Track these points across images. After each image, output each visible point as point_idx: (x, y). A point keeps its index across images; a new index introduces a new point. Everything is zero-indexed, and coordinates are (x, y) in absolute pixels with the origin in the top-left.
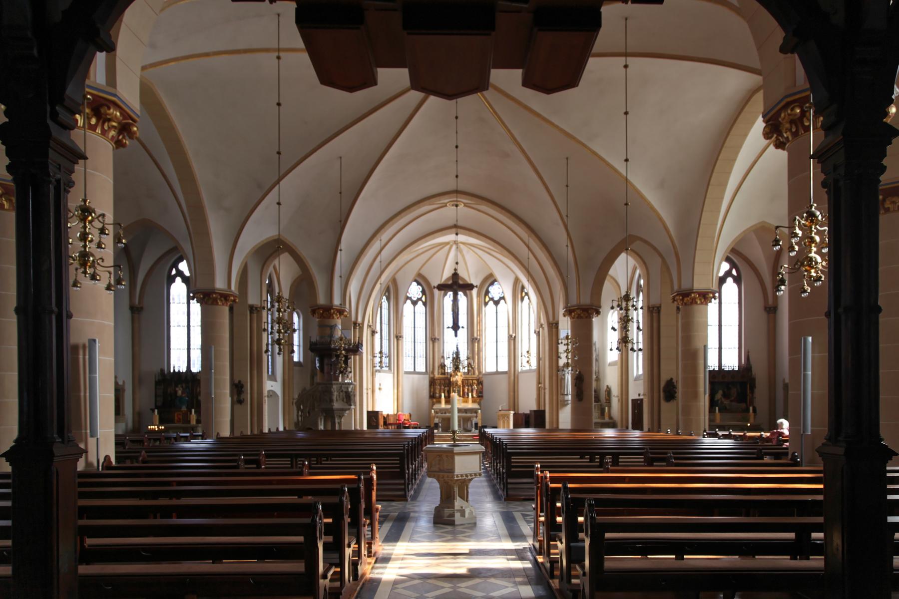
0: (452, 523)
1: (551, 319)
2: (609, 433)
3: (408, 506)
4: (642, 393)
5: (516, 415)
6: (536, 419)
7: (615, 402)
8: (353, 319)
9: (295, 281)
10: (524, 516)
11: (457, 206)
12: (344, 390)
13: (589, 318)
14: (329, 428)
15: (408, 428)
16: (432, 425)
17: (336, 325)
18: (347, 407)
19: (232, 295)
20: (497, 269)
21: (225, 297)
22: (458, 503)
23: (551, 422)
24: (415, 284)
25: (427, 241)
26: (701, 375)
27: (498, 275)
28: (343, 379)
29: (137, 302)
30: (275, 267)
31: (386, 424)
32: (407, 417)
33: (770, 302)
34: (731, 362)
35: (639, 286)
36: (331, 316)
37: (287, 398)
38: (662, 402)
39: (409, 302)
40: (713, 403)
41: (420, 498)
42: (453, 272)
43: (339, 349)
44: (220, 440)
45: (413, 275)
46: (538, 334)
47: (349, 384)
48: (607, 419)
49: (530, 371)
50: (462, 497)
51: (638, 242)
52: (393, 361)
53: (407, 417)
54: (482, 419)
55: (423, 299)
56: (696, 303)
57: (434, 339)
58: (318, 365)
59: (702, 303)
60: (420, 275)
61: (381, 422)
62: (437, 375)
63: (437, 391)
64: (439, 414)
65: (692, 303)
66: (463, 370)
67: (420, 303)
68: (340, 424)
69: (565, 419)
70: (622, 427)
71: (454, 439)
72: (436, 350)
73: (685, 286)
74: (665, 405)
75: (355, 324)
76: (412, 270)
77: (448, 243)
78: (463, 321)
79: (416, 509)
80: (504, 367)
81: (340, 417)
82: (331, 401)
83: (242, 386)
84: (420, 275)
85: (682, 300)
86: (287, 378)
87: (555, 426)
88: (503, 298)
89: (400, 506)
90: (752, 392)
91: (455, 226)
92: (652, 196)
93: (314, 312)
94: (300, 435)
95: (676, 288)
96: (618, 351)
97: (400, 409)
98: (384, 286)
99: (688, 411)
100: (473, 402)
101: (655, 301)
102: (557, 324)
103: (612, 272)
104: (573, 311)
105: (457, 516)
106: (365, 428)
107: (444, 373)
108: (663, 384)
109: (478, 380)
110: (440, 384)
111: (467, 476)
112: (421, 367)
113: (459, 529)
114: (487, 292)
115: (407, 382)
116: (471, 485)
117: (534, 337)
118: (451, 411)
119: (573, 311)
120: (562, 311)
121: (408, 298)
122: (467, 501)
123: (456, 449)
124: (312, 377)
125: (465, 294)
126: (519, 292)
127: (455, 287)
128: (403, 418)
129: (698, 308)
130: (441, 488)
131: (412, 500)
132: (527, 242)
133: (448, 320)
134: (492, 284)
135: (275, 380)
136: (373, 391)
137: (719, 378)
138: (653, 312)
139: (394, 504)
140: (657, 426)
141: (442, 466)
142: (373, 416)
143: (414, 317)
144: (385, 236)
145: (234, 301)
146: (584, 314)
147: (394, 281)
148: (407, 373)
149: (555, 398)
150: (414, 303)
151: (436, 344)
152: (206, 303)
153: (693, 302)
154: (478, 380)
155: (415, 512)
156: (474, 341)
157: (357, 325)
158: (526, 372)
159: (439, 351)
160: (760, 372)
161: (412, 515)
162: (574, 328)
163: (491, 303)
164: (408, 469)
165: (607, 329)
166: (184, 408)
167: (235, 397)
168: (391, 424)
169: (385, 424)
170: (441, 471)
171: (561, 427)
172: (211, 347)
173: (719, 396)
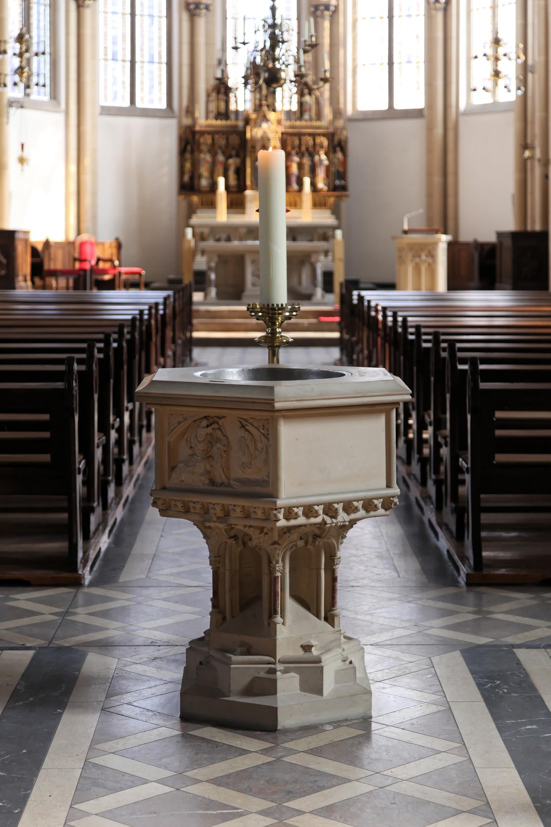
0: (263, 724)
3: (81, 615)
5: (453, 247)
15: (110, 285)
16: (188, 279)
22: (292, 627)
31: (39, 270)
32: (108, 252)
41: (132, 572)
49: (493, 109)
50: (308, 603)
52: (73, 90)
53: (108, 252)
54: (348, 261)
61: (24, 264)
62: (203, 120)
63: (204, 171)
64: (210, 244)
66: (286, 98)
71: (272, 344)
72: (201, 39)
79: (113, 630)
80: (411, 95)
89: (48, 614)
97: (86, 224)
100: (317, 205)
105: (288, 685)
107: (225, 114)
109: (330, 136)
110: (212, 152)
111: (330, 510)
112: (153, 94)
113: (298, 755)
115: (110, 143)
122: (330, 619)
123: (286, 393)
130: (216, 561)
131: (101, 580)
139: (23, 599)
141: (224, 470)
148: (107, 111)
151: (201, 23)
154: (330, 136)
155: (105, 646)
159: (209, 44)
161: (93, 663)
168: (55, 273)
169: (39, 270)
170: (215, 488)
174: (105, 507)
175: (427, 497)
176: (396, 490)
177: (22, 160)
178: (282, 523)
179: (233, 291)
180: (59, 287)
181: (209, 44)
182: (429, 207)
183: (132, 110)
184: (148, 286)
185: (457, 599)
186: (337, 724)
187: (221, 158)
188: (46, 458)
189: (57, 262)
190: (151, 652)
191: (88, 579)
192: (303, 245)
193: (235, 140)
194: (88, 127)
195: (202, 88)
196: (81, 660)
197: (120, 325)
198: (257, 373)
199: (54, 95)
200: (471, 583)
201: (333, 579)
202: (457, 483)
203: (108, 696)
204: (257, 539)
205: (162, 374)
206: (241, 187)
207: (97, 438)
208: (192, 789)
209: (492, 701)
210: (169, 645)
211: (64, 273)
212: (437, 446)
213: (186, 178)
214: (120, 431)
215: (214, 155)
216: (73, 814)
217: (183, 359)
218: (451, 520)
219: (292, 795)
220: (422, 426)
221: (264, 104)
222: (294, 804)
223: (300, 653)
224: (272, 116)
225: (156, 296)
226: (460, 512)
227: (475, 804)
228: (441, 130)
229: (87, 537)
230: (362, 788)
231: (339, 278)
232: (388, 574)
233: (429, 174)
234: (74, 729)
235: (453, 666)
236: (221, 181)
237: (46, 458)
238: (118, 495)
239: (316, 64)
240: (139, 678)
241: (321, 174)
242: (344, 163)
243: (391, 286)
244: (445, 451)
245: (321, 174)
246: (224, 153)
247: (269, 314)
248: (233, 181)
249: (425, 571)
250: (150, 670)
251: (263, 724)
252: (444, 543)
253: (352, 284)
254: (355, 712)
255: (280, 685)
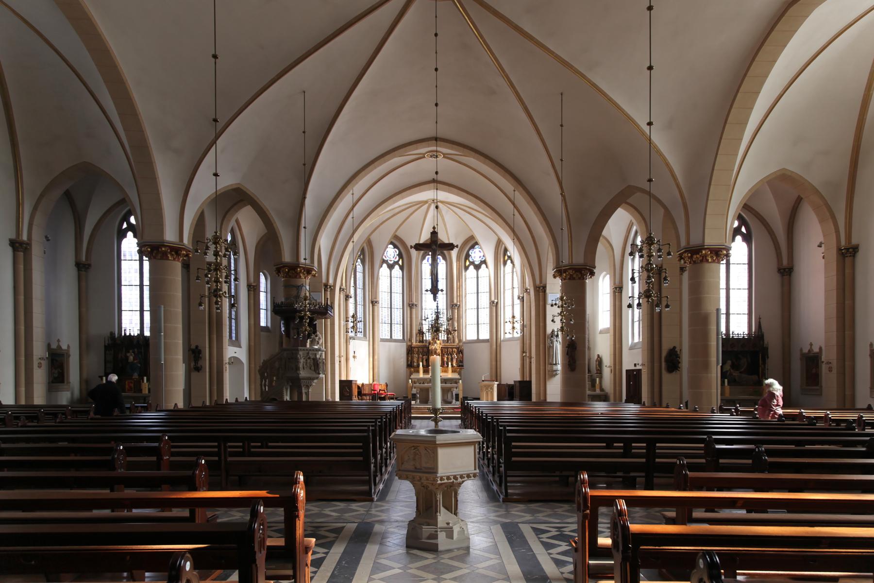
0: (433, 549)
1: (538, 282)
2: (600, 408)
3: (373, 511)
4: (640, 363)
6: (520, 391)
7: (607, 373)
8: (324, 281)
9: (262, 238)
10: (538, 532)
11: (437, 157)
12: (312, 356)
13: (582, 279)
14: (296, 399)
15: (384, 399)
16: (410, 397)
17: (302, 286)
18: (315, 375)
19: (184, 249)
20: (479, 231)
21: (176, 250)
22: (443, 517)
23: (538, 394)
24: (391, 246)
25: (403, 198)
26: (713, 343)
27: (479, 239)
28: (312, 343)
29: (84, 259)
30: (237, 221)
32: (383, 387)
33: (785, 262)
34: (740, 326)
35: (634, 245)
36: (297, 276)
37: (253, 366)
38: (664, 371)
39: (385, 265)
40: (724, 375)
41: (390, 497)
42: (432, 230)
43: (304, 310)
44: (175, 412)
45: (389, 237)
46: (522, 299)
47: (319, 350)
48: (598, 391)
50: (448, 508)
51: (638, 195)
52: (371, 334)
53: (383, 387)
55: (400, 262)
56: (707, 261)
57: (411, 305)
58: (283, 329)
59: (714, 261)
60: (396, 237)
61: (355, 391)
62: (415, 343)
63: (415, 360)
65: (702, 261)
66: (443, 336)
67: (397, 267)
68: (307, 394)
69: (554, 390)
70: (615, 400)
71: (436, 421)
72: (414, 316)
73: (695, 241)
74: (666, 376)
75: (326, 285)
76: (387, 232)
77: (426, 202)
78: (442, 284)
79: (384, 516)
80: (485, 335)
81: (308, 387)
82: (298, 369)
83: (200, 352)
84: (396, 237)
85: (691, 257)
86: (252, 344)
87: (542, 398)
88: (484, 262)
89: (362, 511)
90: (764, 363)
91: (434, 181)
92: (659, 139)
93: (278, 271)
94: (269, 408)
95: (683, 243)
96: (614, 315)
98: (358, 248)
99: (697, 383)
100: (453, 372)
101: (655, 262)
102: (544, 287)
103: (604, 233)
104: (565, 271)
105: (442, 536)
106: (337, 399)
107: (422, 341)
108: (664, 354)
110: (417, 353)
111: (455, 477)
112: (398, 334)
113: (445, 560)
114: (468, 256)
115: (383, 351)
116: (461, 491)
117: (517, 302)
118: (432, 380)
119: (565, 271)
120: (550, 271)
121: (384, 261)
122: (456, 514)
123: (440, 438)
124: (281, 344)
125: (444, 258)
126: (502, 255)
127: (434, 247)
128: (378, 388)
129: (709, 267)
130: (417, 494)
132: (512, 197)
133: (427, 284)
134: (473, 247)
135: (240, 347)
136: (347, 360)
137: (730, 344)
138: (654, 276)
139: (354, 506)
140: (657, 400)
141: (420, 462)
142: (346, 385)
143: (390, 281)
144: (358, 187)
145: (187, 255)
146: (577, 276)
147: (369, 242)
148: (383, 340)
149: (542, 367)
150: (391, 267)
151: (414, 311)
152: (155, 258)
153: (704, 259)
154: (458, 348)
155: (381, 522)
156: (454, 306)
157: (328, 288)
158: (509, 340)
159: (417, 318)
160: (773, 340)
161: (377, 528)
162: (565, 289)
163: (472, 267)
164: (375, 457)
165: (601, 290)
166: (136, 376)
167: (192, 364)
168: (365, 395)
169: (360, 393)
170: (417, 470)
171: (548, 400)
172: (160, 307)
173: (728, 367)
174: (381, 475)
175: (489, 471)
176: (478, 471)
177: (354, 357)
178: (439, 482)
179: (425, 400)
180: (367, 400)
181: (417, 318)
182: (491, 372)
183: (391, 340)
184: (396, 399)
185: (499, 507)
186: (458, 549)
188: (361, 458)
189: (366, 391)
190: (397, 524)
191: (376, 499)
192: (448, 385)
193: (425, 349)
194: (376, 346)
195: (414, 332)
196: (373, 527)
197: (386, 413)
198: (431, 432)
199: (365, 335)
200: (504, 501)
201: (456, 501)
202: (500, 467)
203: (382, 539)
204: (431, 487)
205: (399, 432)
206: (428, 365)
207: (379, 451)
208: (409, 571)
209: (511, 541)
210: (402, 522)
211: (368, 395)
212: (493, 454)
214: (386, 449)
216: (370, 579)
217: (408, 425)
218: (498, 480)
219: (443, 573)
220: (488, 448)
221: (435, 338)
222: (443, 576)
223: (446, 525)
224: (438, 342)
225: (399, 402)
226: (500, 477)
227: (505, 577)
228: (495, 345)
229: (375, 485)
230: (467, 571)
231: (461, 396)
232: (476, 498)
233: (491, 361)
234: (371, 549)
235: (498, 530)
237: (361, 458)
238: (386, 470)
239: (453, 325)
240: (393, 533)
241: (455, 361)
243: (478, 399)
244: (495, 456)
245: (455, 361)
247: (435, 411)
249: (489, 496)
250: (396, 530)
251: (433, 549)
252: (495, 487)
253: (465, 398)
254: (464, 545)
255: (439, 536)
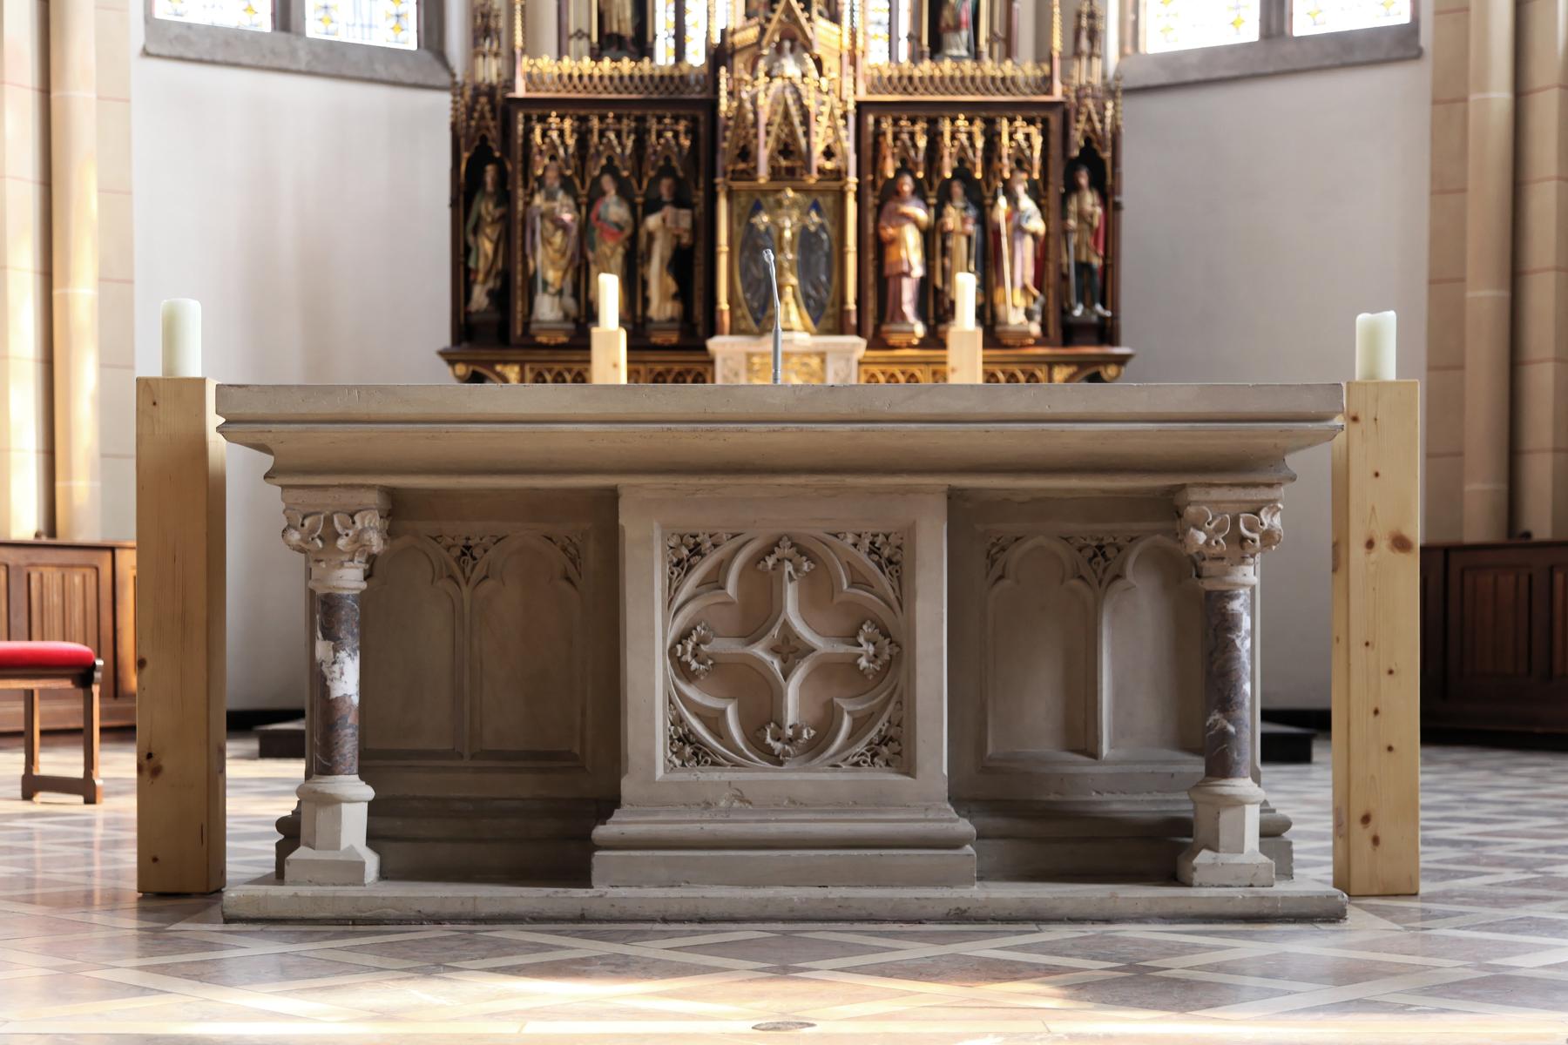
63: (548, 264)
148: (179, 45)
187: (614, 209)
193: (673, 136)
213: (479, 298)
215: (588, 201)
236: (608, 289)
241: (1020, 263)
242: (1109, 236)
245: (1020, 263)
246: (624, 192)
248: (661, 306)
